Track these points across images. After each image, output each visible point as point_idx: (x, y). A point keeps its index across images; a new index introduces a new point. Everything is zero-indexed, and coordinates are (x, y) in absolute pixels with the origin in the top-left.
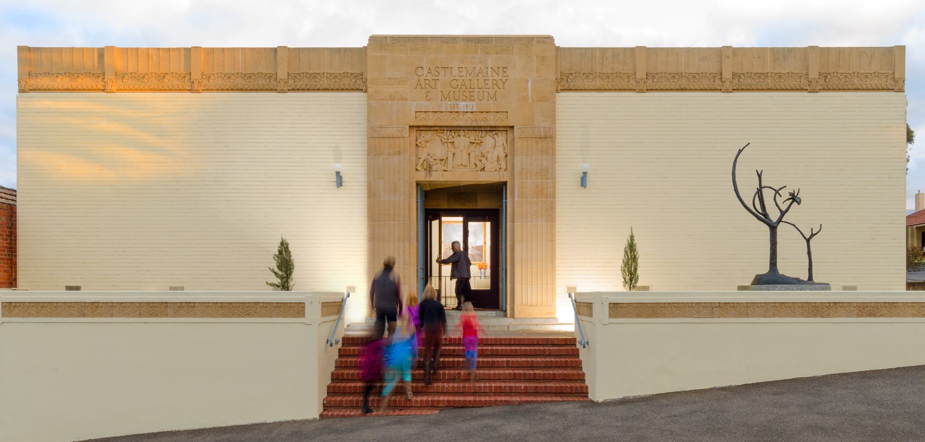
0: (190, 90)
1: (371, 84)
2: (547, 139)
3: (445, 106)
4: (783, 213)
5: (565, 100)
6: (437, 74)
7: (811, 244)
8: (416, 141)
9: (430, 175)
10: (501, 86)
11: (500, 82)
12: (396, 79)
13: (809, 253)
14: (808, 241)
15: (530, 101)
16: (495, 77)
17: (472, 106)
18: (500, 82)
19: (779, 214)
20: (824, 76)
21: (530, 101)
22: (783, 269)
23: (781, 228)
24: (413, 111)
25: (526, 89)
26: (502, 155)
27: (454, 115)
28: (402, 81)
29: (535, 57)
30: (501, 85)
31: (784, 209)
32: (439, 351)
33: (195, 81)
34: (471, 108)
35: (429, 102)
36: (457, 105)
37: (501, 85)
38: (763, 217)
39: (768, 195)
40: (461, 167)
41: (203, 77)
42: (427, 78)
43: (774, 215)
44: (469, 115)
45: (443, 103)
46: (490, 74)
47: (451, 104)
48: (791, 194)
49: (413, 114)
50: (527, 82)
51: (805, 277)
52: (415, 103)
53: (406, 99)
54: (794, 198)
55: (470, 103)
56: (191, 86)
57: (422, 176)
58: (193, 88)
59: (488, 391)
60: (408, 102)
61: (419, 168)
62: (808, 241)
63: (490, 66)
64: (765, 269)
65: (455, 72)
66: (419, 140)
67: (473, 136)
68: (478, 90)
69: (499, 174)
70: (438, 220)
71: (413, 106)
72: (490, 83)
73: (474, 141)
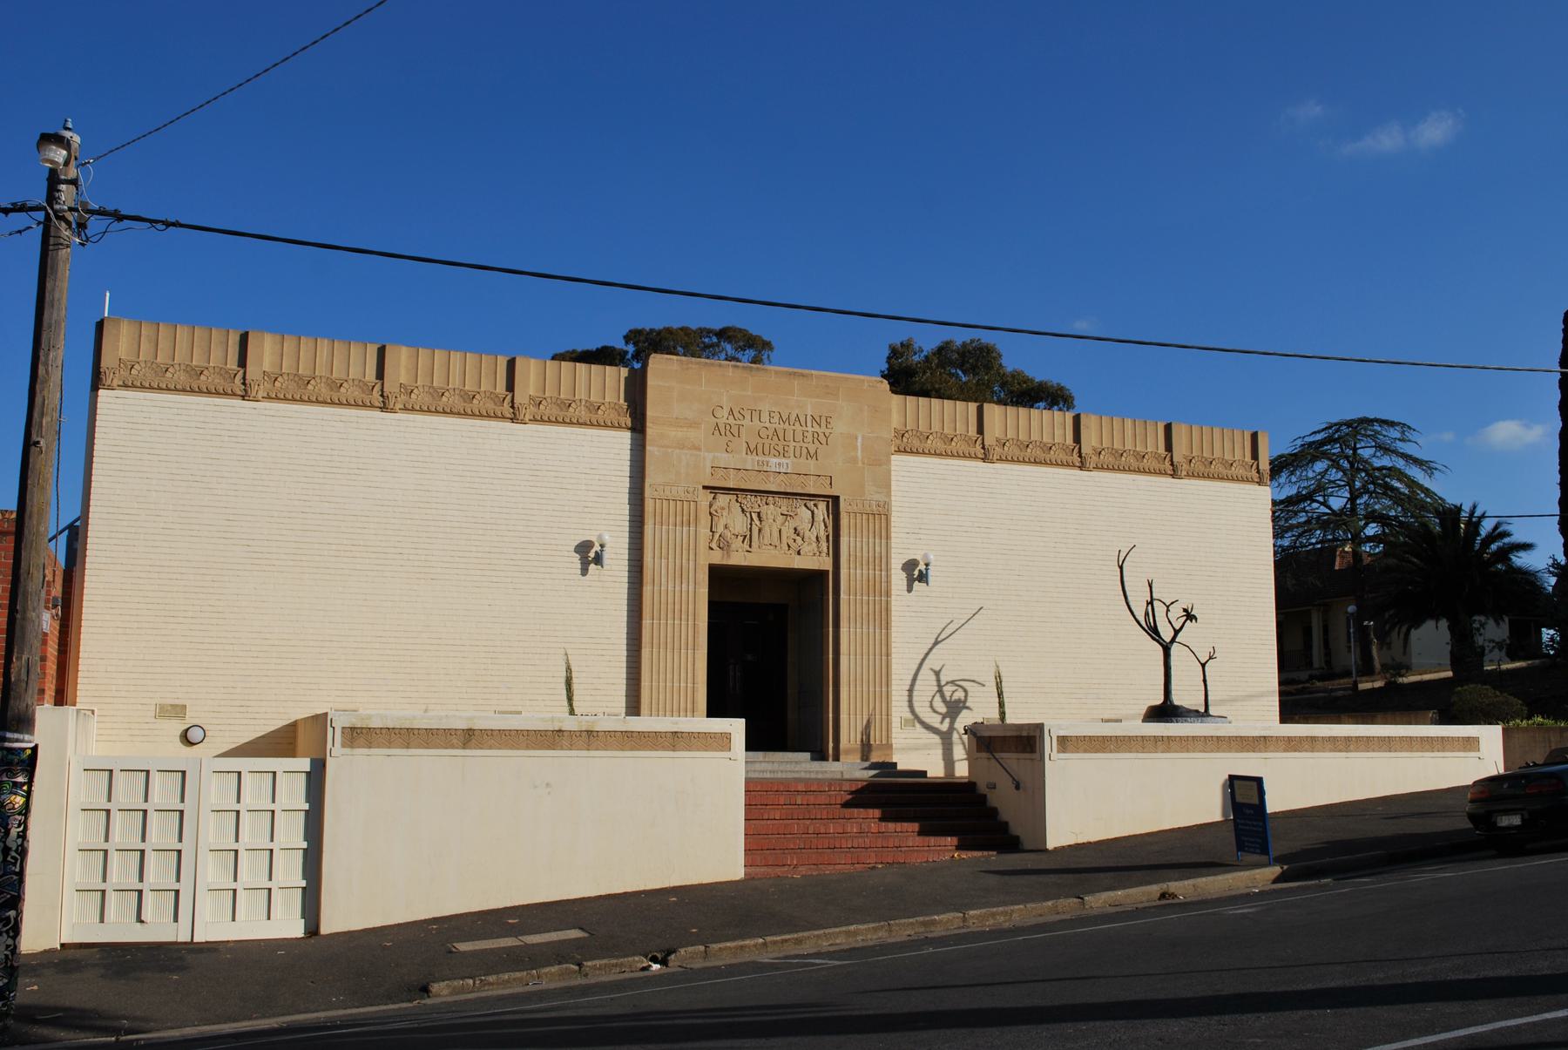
0: (511, 419)
1: (653, 423)
2: (881, 517)
3: (751, 461)
4: (1177, 632)
5: (901, 465)
6: (741, 417)
7: (1206, 668)
8: (710, 507)
9: (729, 556)
10: (824, 441)
11: (821, 435)
12: (686, 419)
13: (1205, 681)
14: (1203, 665)
15: (860, 464)
16: (817, 428)
17: (787, 464)
18: (821, 435)
19: (1172, 633)
20: (641, 445)
21: (860, 464)
22: (1177, 700)
23: (1175, 649)
24: (709, 465)
25: (856, 448)
26: (822, 535)
27: (762, 475)
28: (695, 423)
29: (866, 407)
30: (823, 440)
31: (1177, 628)
32: (664, 954)
33: (390, 396)
34: (785, 467)
35: (731, 455)
36: (768, 462)
37: (823, 440)
38: (1153, 632)
39: (1160, 609)
40: (770, 547)
41: (266, 378)
42: (727, 421)
43: (1167, 634)
44: (781, 477)
45: (749, 457)
46: (809, 424)
47: (758, 461)
48: (1185, 610)
49: (708, 470)
50: (856, 438)
51: (1202, 710)
52: (710, 456)
53: (699, 449)
54: (1189, 616)
55: (784, 461)
56: (245, 390)
57: (718, 558)
58: (387, 405)
59: (832, 831)
60: (702, 453)
61: (714, 545)
62: (1203, 665)
63: (809, 413)
64: (1158, 699)
65: (765, 417)
66: (714, 507)
67: (784, 505)
68: (794, 444)
69: (819, 561)
70: (325, 929)
71: (708, 458)
72: (809, 435)
73: (787, 513)
